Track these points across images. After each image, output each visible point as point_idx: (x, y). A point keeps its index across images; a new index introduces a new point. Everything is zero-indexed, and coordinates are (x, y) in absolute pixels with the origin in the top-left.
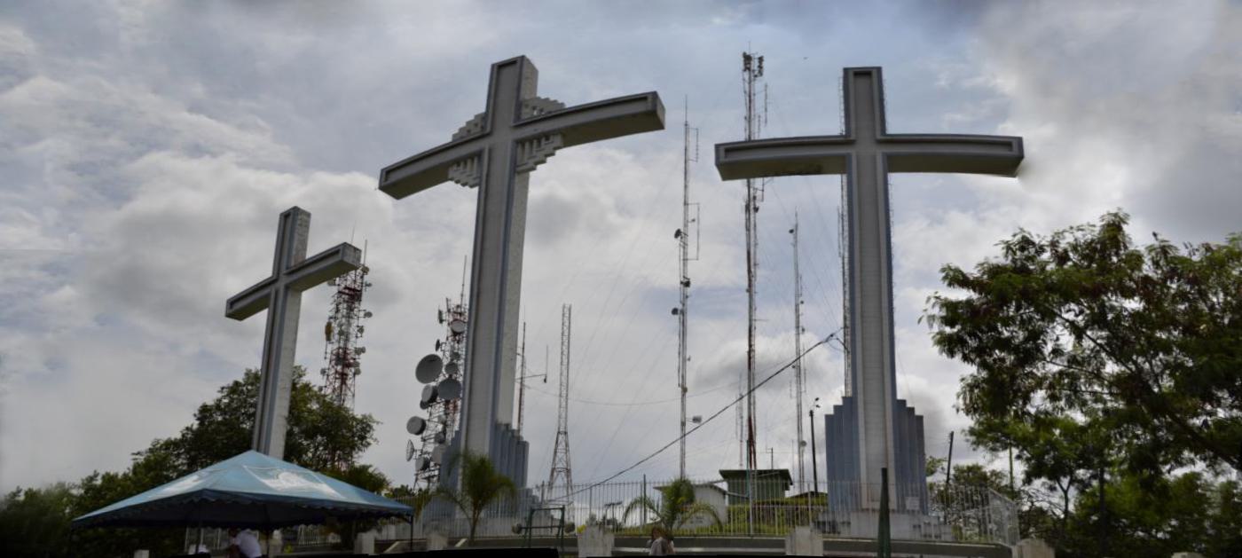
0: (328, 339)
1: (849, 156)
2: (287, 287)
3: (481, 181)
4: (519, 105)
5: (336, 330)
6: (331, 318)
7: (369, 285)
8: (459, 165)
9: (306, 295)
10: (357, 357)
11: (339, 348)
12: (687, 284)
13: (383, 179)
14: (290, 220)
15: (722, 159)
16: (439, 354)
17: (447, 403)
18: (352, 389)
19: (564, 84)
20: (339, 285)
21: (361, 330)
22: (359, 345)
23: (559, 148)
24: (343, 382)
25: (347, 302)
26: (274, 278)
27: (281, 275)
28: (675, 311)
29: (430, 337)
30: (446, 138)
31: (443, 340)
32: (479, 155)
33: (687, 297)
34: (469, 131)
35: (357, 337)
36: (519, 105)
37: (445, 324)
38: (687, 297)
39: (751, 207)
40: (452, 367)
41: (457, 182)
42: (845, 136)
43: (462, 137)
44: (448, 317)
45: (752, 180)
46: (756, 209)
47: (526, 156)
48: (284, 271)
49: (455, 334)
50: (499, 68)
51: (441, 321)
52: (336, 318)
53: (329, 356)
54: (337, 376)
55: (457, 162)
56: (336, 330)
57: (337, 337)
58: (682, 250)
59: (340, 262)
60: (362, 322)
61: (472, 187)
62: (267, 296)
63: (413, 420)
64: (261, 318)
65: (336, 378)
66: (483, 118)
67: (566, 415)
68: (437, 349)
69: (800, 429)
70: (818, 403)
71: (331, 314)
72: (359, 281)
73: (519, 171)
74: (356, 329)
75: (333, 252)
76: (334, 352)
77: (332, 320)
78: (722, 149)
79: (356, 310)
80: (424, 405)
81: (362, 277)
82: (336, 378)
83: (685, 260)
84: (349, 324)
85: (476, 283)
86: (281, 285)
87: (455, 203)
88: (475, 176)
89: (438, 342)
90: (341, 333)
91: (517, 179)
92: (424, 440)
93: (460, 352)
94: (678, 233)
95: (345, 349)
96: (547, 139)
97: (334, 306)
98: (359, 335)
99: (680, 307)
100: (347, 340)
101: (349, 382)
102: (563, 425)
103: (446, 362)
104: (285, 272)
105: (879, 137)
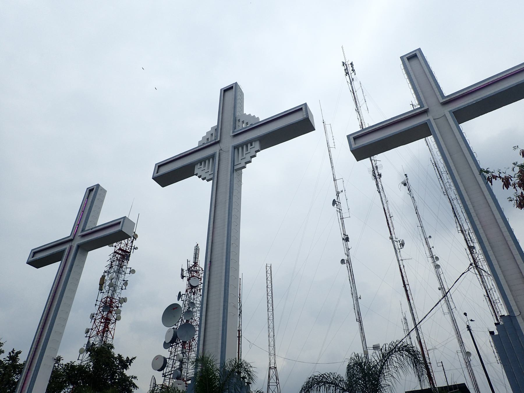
0: (101, 289)
1: (429, 120)
2: (79, 246)
3: (214, 176)
4: (235, 120)
5: (107, 283)
6: (105, 272)
7: (136, 248)
8: (201, 165)
9: (92, 254)
10: (120, 305)
11: (108, 297)
12: (347, 239)
13: (156, 172)
14: (93, 193)
15: (354, 146)
16: (180, 303)
17: (184, 343)
18: (112, 332)
19: (259, 106)
20: (115, 246)
21: (126, 283)
22: (122, 296)
23: (258, 151)
24: (106, 326)
25: (119, 260)
26: (71, 238)
27: (77, 237)
28: (343, 261)
29: (172, 288)
30: (194, 145)
31: (183, 292)
32: (213, 156)
33: (349, 249)
34: (208, 139)
35: (122, 289)
36: (235, 120)
37: (185, 279)
38: (349, 249)
39: (377, 176)
40: (189, 312)
41: (200, 177)
42: (421, 108)
43: (204, 144)
44: (186, 274)
45: (372, 157)
46: (380, 175)
47: (240, 158)
48: (79, 234)
49: (192, 287)
50: (225, 91)
51: (183, 277)
52: (109, 272)
53: (98, 303)
54: (103, 321)
55: (200, 162)
56: (107, 283)
57: (107, 287)
58: (339, 213)
59: (118, 234)
60: (128, 277)
61: (208, 181)
62: (63, 251)
63: (157, 358)
64: (54, 268)
65: (101, 322)
66: (216, 129)
67: (275, 361)
68: (178, 300)
69: (461, 343)
70: (469, 317)
71: (106, 269)
72: (130, 244)
73: (237, 170)
74: (123, 282)
75: (116, 223)
76: (103, 300)
77: (106, 274)
78: (351, 137)
79: (124, 267)
80: (166, 345)
81: (132, 242)
82: (101, 322)
83: (342, 219)
84: (118, 278)
85: (221, 116)
86: (75, 244)
87: (196, 191)
88: (210, 173)
89: (180, 293)
90: (110, 285)
91: (235, 174)
92: (164, 376)
93: (195, 302)
94: (334, 202)
95: (112, 298)
96: (251, 145)
97: (109, 263)
98: (124, 287)
99: (345, 258)
100: (114, 291)
101: (111, 326)
102: (273, 361)
103: (184, 309)
104: (80, 234)
105: (442, 101)
